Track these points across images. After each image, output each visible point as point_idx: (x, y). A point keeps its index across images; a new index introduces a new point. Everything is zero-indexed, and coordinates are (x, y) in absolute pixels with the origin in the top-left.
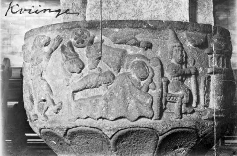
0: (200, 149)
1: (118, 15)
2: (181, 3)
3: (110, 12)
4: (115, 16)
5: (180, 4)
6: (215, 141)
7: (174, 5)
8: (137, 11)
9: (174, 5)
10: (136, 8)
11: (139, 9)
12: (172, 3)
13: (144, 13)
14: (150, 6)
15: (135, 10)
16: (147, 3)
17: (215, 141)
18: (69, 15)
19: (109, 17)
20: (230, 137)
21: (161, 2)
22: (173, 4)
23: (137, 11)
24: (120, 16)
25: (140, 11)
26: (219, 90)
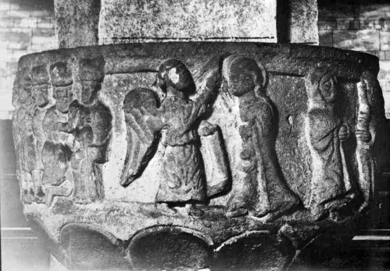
2: (263, 7)
3: (142, 21)
8: (189, 20)
10: (186, 15)
11: (193, 17)
15: (186, 18)
19: (141, 29)
21: (230, 5)
22: (250, 10)
23: (189, 20)
24: (160, 28)
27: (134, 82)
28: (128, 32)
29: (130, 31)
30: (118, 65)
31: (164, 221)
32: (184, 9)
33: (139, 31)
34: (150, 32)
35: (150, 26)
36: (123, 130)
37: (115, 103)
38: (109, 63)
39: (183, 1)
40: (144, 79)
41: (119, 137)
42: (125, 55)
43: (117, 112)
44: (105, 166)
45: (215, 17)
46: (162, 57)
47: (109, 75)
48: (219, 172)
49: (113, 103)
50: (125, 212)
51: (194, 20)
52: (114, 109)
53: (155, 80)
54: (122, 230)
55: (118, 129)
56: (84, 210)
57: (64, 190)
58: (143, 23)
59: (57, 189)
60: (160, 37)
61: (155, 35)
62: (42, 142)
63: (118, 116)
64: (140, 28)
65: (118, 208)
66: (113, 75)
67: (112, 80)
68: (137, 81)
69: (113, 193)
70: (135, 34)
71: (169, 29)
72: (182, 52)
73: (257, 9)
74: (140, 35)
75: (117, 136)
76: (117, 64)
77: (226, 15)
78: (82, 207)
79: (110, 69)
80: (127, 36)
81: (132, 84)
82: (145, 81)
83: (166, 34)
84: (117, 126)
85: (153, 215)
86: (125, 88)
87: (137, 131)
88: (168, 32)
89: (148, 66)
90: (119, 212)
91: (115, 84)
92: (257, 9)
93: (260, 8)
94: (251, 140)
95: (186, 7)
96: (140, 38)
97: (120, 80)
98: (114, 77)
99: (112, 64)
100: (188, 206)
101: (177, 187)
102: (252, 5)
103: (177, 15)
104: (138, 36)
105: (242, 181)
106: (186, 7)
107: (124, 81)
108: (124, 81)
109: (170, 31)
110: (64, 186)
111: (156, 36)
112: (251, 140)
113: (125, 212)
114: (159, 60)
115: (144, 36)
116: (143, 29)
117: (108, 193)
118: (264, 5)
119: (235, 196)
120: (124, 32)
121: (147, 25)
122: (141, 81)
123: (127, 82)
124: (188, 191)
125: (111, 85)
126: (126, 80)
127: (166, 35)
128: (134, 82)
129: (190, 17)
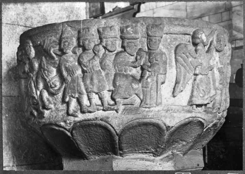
0: (195, 135)
1: (25, 19)
2: (80, 15)
3: (17, 14)
4: (22, 19)
5: (79, 16)
6: (186, 173)
7: (75, 17)
8: (42, 17)
9: (75, 17)
10: (41, 14)
11: (44, 15)
12: (72, 14)
13: (48, 20)
14: (54, 13)
15: (40, 16)
16: (51, 10)
17: (186, 173)
18: (18, 45)
19: (17, 19)
20: (187, 171)
21: (64, 11)
22: (73, 16)
23: (42, 17)
24: (27, 20)
25: (45, 18)
26: (69, 45)
27: (179, 40)
28: (9, 20)
29: (11, 19)
30: (171, 29)
31: (193, 115)
32: (39, 10)
33: (16, 20)
34: (22, 22)
35: (22, 18)
36: (173, 66)
37: (168, 51)
38: (166, 28)
39: (101, 1)
40: (184, 39)
41: (171, 70)
42: (177, 24)
43: (170, 56)
44: (163, 86)
45: (56, 18)
46: (194, 27)
47: (166, 35)
48: (213, 90)
49: (167, 51)
50: (176, 111)
51: (45, 17)
52: (168, 54)
53: (189, 40)
54: (173, 121)
55: (171, 66)
56: (150, 111)
57: (133, 101)
58: (18, 15)
59: (127, 100)
60: (28, 26)
61: (25, 24)
62: (112, 73)
63: (171, 58)
64: (16, 18)
65: (171, 109)
66: (168, 35)
67: (168, 38)
68: (180, 39)
69: (167, 101)
70: (13, 22)
71: (32, 21)
72: (39, 41)
73: (77, 16)
74: (17, 24)
75: (170, 69)
76: (171, 29)
77: (62, 17)
78: (147, 109)
79: (168, 31)
80: (9, 23)
81: (178, 41)
82: (184, 40)
83: (31, 25)
84: (169, 64)
85: (189, 111)
86: (175, 43)
87: (185, 67)
88: (32, 24)
89: (187, 31)
90: (173, 111)
91: (169, 40)
92: (77, 16)
93: (78, 16)
94: (224, 75)
95: (40, 8)
96: (17, 25)
97: (171, 38)
98: (168, 36)
99: (168, 28)
100: (203, 107)
101: (203, 96)
102: (74, 13)
103: (36, 13)
104: (15, 24)
105: (219, 95)
106: (40, 8)
107: (174, 39)
108: (174, 39)
109: (32, 23)
110: (133, 99)
111: (26, 25)
112: (224, 75)
113: (176, 111)
114: (192, 29)
115: (19, 24)
116: (18, 20)
117: (164, 101)
118: (80, 14)
119: (216, 103)
120: (7, 20)
121: (20, 17)
122: (182, 39)
123: (175, 39)
124: (207, 99)
125: (167, 40)
126: (175, 38)
127: (30, 25)
128: (179, 40)
129: (43, 15)
